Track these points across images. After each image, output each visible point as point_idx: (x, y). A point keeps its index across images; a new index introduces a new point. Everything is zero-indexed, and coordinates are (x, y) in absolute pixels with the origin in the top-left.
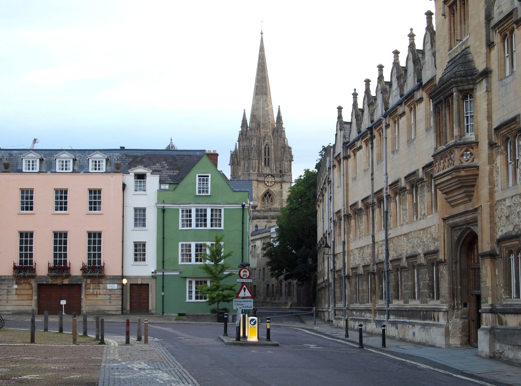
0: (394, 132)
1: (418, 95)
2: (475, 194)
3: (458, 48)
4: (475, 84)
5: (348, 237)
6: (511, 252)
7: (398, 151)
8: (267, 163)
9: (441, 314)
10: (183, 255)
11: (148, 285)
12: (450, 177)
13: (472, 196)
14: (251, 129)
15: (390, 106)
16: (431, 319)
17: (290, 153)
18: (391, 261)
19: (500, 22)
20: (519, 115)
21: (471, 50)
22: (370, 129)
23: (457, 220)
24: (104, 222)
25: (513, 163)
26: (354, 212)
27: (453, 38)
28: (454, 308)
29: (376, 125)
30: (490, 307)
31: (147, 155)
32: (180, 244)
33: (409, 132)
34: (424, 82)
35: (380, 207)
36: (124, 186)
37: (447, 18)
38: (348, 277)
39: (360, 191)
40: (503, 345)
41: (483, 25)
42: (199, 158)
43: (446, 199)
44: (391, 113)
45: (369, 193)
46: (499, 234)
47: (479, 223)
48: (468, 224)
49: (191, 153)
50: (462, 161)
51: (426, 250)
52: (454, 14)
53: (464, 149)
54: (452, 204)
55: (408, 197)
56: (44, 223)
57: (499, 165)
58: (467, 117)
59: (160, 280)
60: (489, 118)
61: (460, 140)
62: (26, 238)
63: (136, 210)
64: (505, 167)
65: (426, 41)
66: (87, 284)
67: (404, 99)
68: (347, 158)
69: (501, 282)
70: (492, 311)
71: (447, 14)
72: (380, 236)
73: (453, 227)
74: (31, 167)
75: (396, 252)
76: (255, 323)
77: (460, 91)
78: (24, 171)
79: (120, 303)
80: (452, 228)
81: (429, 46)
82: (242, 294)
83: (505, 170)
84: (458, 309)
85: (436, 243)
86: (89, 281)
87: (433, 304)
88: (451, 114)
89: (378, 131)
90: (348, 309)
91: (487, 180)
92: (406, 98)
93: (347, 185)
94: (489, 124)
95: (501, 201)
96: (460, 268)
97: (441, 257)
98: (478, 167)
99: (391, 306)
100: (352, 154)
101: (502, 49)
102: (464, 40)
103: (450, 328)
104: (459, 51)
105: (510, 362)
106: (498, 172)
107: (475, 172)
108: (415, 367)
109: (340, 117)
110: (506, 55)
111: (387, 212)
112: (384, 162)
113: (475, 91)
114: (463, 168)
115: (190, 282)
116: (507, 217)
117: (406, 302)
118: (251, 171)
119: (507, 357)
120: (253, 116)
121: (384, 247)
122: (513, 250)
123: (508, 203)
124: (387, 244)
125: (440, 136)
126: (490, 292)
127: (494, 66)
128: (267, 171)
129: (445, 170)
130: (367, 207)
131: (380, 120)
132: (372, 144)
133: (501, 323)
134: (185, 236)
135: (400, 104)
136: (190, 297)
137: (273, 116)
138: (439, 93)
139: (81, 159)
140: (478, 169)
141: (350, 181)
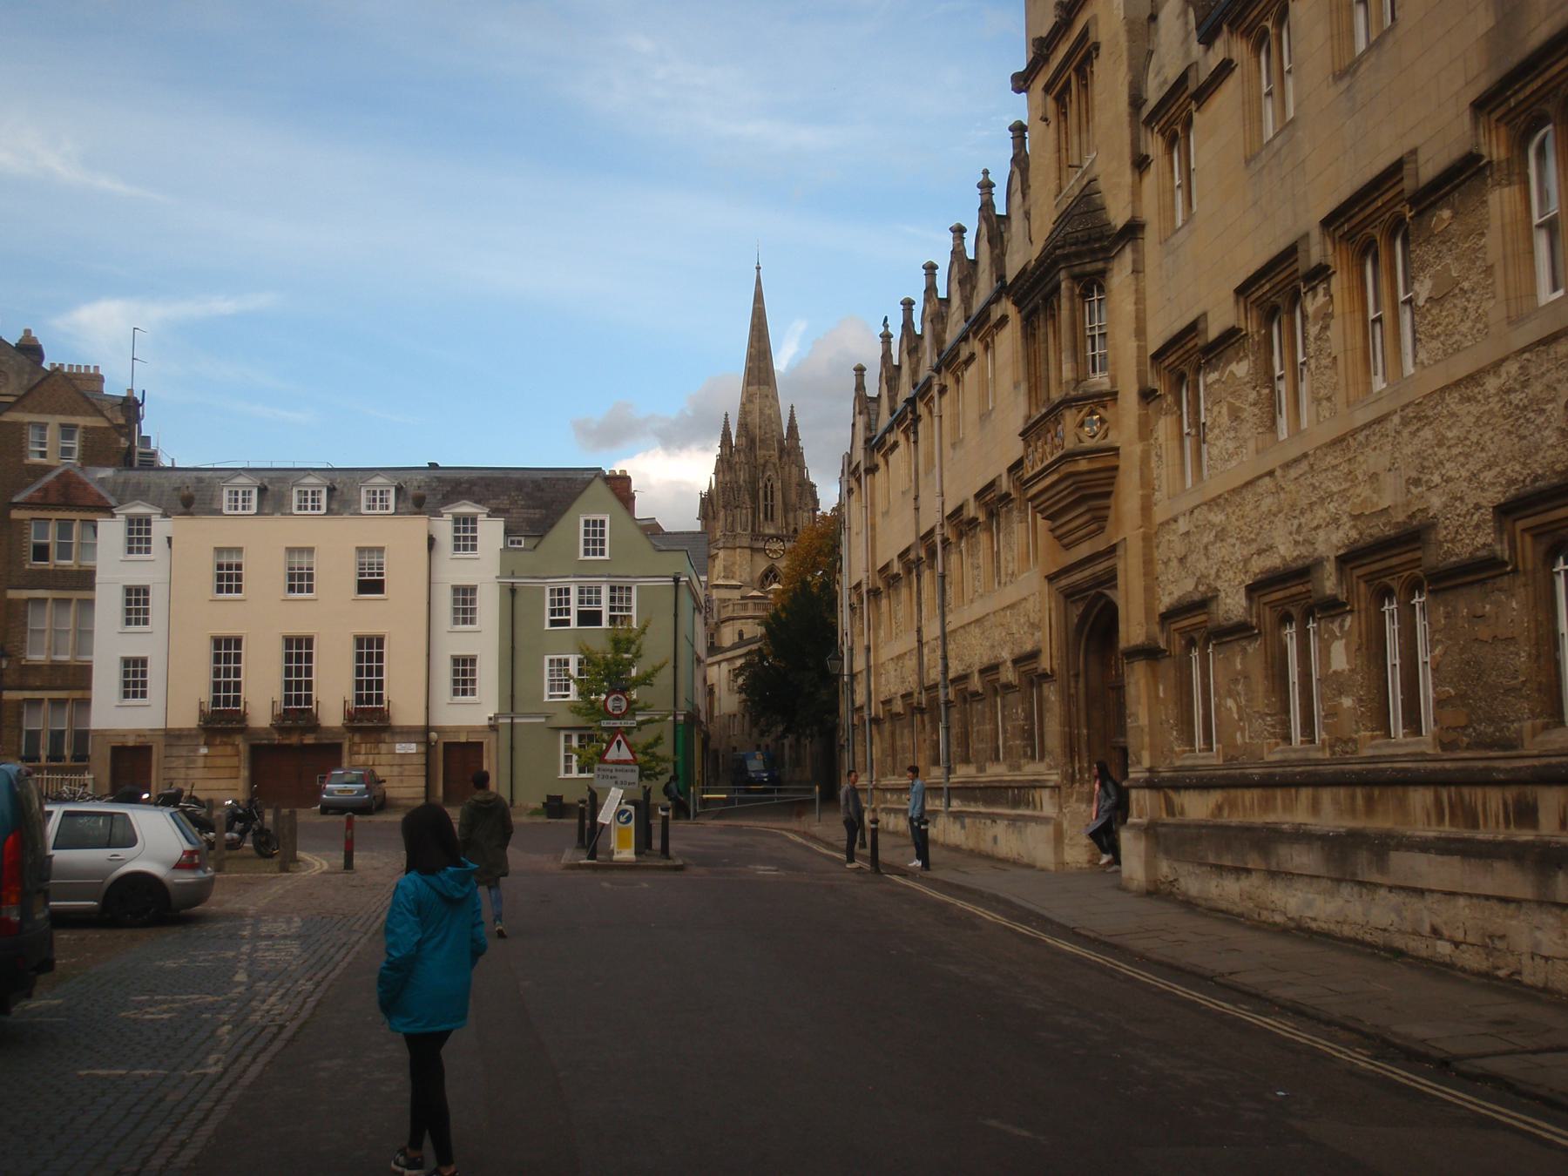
0: (955, 401)
2: (1112, 514)
3: (1073, 185)
4: (1108, 259)
5: (877, 636)
6: (1191, 643)
7: (962, 441)
8: (769, 517)
9: (1046, 794)
12: (1054, 477)
13: (1105, 518)
14: (738, 451)
16: (1027, 805)
17: (814, 494)
18: (953, 681)
20: (1205, 314)
21: (1101, 184)
22: (911, 402)
23: (1077, 577)
24: (394, 616)
25: (1193, 432)
26: (889, 580)
27: (1064, 165)
28: (1072, 780)
29: (923, 391)
30: (1147, 774)
31: (482, 478)
32: (547, 658)
33: (984, 396)
35: (931, 567)
36: (431, 542)
37: (1053, 125)
38: (876, 721)
39: (897, 537)
40: (1176, 865)
41: (1125, 119)
42: (589, 482)
43: (1052, 530)
45: (910, 539)
46: (1165, 602)
47: (1120, 581)
48: (1100, 584)
50: (1082, 436)
51: (1017, 651)
52: (1065, 114)
54: (1066, 541)
55: (983, 538)
56: (263, 620)
57: (1162, 439)
58: (1093, 337)
59: (505, 734)
60: (1140, 332)
61: (1075, 389)
62: (227, 650)
63: (456, 589)
64: (1176, 443)
65: (1013, 188)
66: (352, 745)
67: (971, 326)
68: (872, 470)
69: (1169, 713)
71: (1051, 115)
72: (932, 630)
73: (1069, 595)
74: (240, 504)
75: (961, 660)
76: (629, 819)
77: (1075, 278)
78: (225, 511)
79: (422, 782)
80: (1067, 596)
82: (612, 754)
83: (1177, 452)
84: (1082, 782)
86: (357, 739)
87: (1031, 770)
88: (1057, 333)
89: (926, 404)
90: (876, 788)
91: (1136, 476)
92: (975, 321)
93: (873, 527)
94: (1139, 347)
95: (1167, 522)
96: (1087, 687)
97: (1045, 664)
98: (1117, 449)
99: (954, 779)
101: (1168, 169)
102: (1086, 165)
103: (1065, 825)
104: (1077, 191)
105: (1189, 905)
106: (1160, 457)
108: (971, 922)
109: (860, 387)
110: (1177, 182)
111: (943, 577)
112: (937, 468)
113: (1108, 275)
114: (1084, 453)
115: (568, 738)
116: (1182, 560)
117: (981, 769)
118: (739, 530)
119: (1185, 894)
120: (743, 426)
121: (939, 653)
122: (1196, 636)
123: (1183, 525)
124: (944, 644)
126: (1147, 739)
127: (1149, 213)
128: (770, 531)
129: (1046, 463)
130: (909, 572)
132: (916, 433)
133: (1170, 809)
135: (964, 338)
136: (568, 769)
137: (780, 425)
139: (340, 490)
140: (1117, 455)
141: (878, 519)
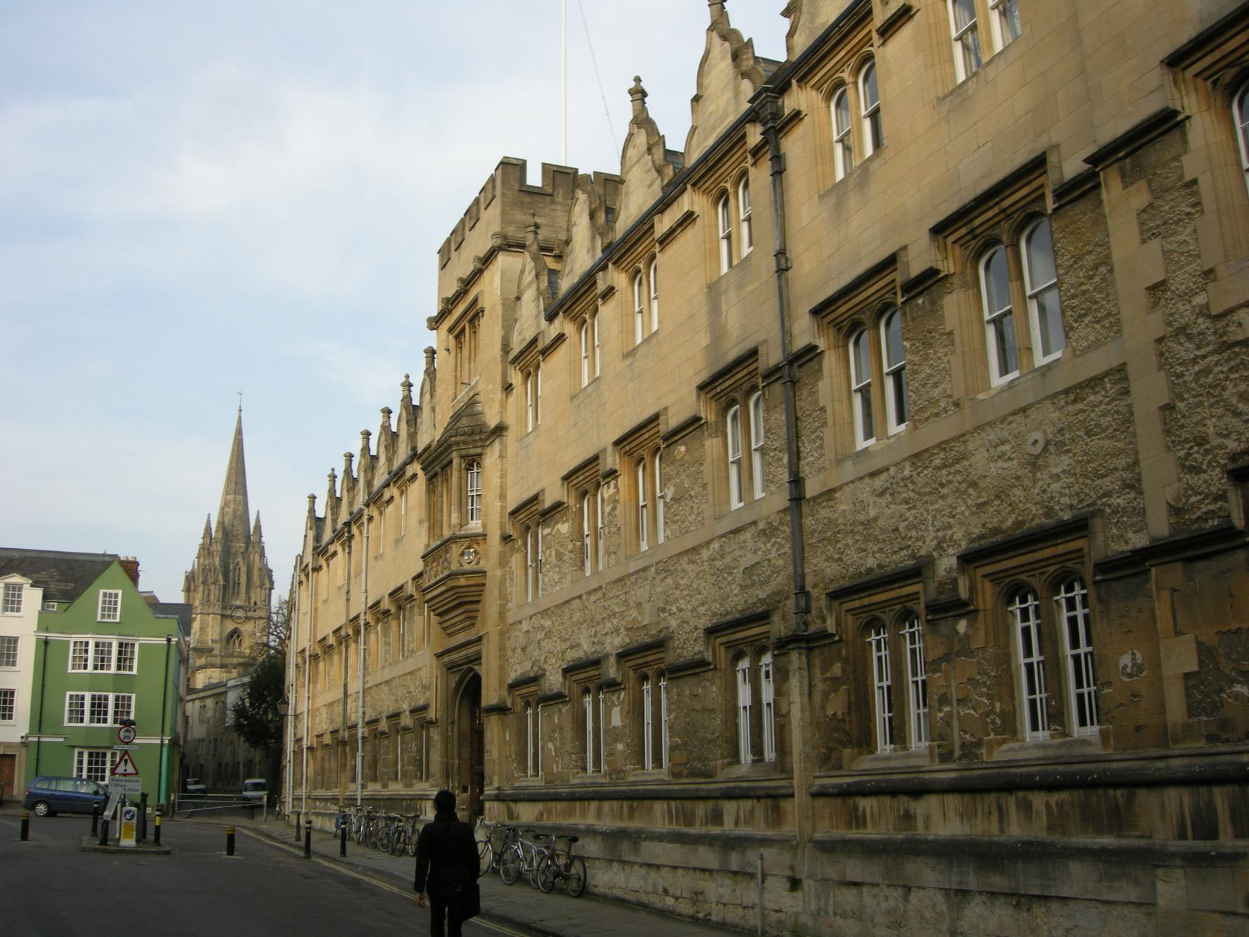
1: (410, 471)
2: (480, 614)
6: (528, 704)
10: (71, 711)
11: (13, 756)
13: (476, 617)
19: (522, 353)
22: (348, 524)
27: (458, 382)
29: (356, 518)
34: (419, 450)
35: (356, 642)
37: (453, 354)
41: (499, 359)
44: (375, 499)
46: (512, 676)
47: (484, 660)
49: (95, 559)
53: (466, 545)
55: (394, 624)
60: (503, 497)
64: (523, 572)
68: (317, 569)
70: (498, 798)
73: (451, 668)
80: (449, 669)
81: (427, 396)
88: (449, 492)
91: (496, 592)
93: (316, 610)
95: (515, 623)
97: (431, 714)
100: (324, 564)
107: (481, 581)
108: (373, 891)
109: (312, 510)
114: (463, 574)
115: (81, 754)
116: (524, 649)
120: (221, 524)
122: (531, 699)
123: (525, 626)
125: (433, 523)
127: (510, 420)
132: (350, 547)
133: (511, 815)
134: (81, 683)
138: (433, 461)
141: (320, 604)
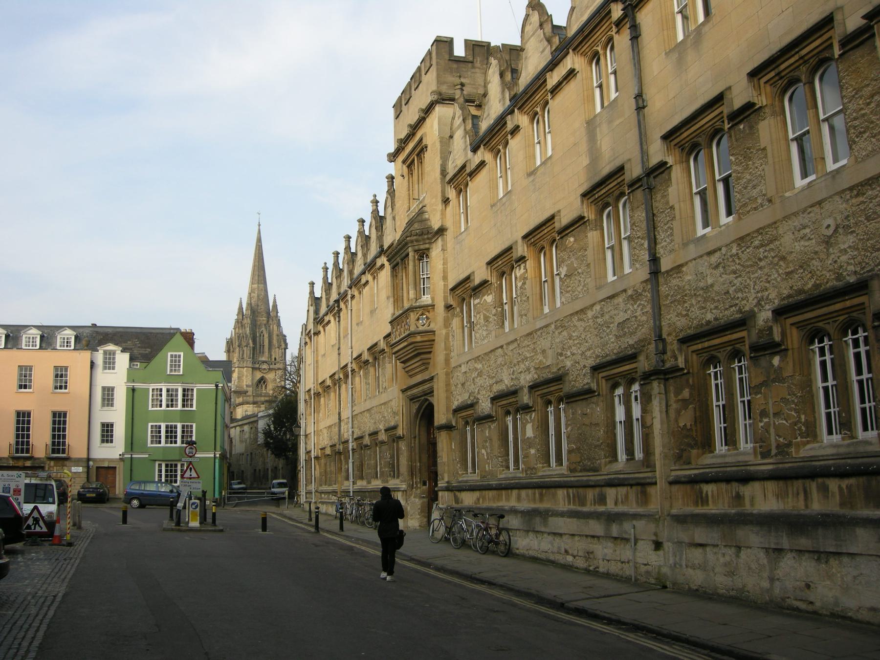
1: (379, 262)
2: (431, 361)
6: (467, 423)
10: (152, 436)
15: (355, 276)
17: (285, 341)
19: (455, 176)
20: (473, 272)
22: (337, 301)
23: (415, 391)
29: (343, 297)
32: (150, 424)
35: (346, 383)
36: (92, 365)
37: (406, 178)
41: (439, 181)
42: (174, 334)
46: (455, 404)
47: (435, 393)
48: (426, 395)
53: (420, 313)
55: (372, 370)
59: (128, 463)
60: (445, 278)
64: (461, 331)
68: (317, 333)
73: (412, 399)
76: (197, 507)
80: (411, 400)
81: (389, 210)
84: (417, 488)
85: (397, 417)
86: (52, 463)
91: (443, 345)
93: (317, 362)
97: (400, 432)
100: (321, 329)
107: (431, 338)
109: (312, 292)
112: (349, 336)
115: (160, 465)
116: (463, 385)
120: (249, 304)
123: (464, 369)
125: (397, 298)
126: (446, 468)
127: (449, 224)
131: (346, 291)
132: (339, 317)
133: (457, 500)
134: (157, 416)
141: (320, 358)
